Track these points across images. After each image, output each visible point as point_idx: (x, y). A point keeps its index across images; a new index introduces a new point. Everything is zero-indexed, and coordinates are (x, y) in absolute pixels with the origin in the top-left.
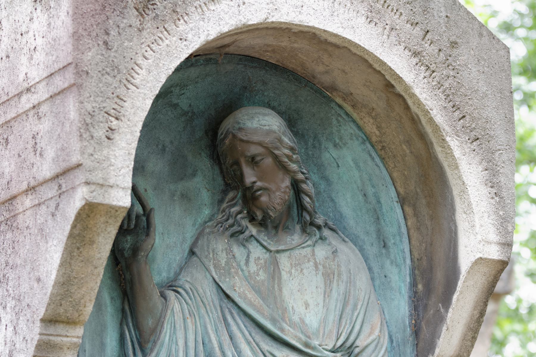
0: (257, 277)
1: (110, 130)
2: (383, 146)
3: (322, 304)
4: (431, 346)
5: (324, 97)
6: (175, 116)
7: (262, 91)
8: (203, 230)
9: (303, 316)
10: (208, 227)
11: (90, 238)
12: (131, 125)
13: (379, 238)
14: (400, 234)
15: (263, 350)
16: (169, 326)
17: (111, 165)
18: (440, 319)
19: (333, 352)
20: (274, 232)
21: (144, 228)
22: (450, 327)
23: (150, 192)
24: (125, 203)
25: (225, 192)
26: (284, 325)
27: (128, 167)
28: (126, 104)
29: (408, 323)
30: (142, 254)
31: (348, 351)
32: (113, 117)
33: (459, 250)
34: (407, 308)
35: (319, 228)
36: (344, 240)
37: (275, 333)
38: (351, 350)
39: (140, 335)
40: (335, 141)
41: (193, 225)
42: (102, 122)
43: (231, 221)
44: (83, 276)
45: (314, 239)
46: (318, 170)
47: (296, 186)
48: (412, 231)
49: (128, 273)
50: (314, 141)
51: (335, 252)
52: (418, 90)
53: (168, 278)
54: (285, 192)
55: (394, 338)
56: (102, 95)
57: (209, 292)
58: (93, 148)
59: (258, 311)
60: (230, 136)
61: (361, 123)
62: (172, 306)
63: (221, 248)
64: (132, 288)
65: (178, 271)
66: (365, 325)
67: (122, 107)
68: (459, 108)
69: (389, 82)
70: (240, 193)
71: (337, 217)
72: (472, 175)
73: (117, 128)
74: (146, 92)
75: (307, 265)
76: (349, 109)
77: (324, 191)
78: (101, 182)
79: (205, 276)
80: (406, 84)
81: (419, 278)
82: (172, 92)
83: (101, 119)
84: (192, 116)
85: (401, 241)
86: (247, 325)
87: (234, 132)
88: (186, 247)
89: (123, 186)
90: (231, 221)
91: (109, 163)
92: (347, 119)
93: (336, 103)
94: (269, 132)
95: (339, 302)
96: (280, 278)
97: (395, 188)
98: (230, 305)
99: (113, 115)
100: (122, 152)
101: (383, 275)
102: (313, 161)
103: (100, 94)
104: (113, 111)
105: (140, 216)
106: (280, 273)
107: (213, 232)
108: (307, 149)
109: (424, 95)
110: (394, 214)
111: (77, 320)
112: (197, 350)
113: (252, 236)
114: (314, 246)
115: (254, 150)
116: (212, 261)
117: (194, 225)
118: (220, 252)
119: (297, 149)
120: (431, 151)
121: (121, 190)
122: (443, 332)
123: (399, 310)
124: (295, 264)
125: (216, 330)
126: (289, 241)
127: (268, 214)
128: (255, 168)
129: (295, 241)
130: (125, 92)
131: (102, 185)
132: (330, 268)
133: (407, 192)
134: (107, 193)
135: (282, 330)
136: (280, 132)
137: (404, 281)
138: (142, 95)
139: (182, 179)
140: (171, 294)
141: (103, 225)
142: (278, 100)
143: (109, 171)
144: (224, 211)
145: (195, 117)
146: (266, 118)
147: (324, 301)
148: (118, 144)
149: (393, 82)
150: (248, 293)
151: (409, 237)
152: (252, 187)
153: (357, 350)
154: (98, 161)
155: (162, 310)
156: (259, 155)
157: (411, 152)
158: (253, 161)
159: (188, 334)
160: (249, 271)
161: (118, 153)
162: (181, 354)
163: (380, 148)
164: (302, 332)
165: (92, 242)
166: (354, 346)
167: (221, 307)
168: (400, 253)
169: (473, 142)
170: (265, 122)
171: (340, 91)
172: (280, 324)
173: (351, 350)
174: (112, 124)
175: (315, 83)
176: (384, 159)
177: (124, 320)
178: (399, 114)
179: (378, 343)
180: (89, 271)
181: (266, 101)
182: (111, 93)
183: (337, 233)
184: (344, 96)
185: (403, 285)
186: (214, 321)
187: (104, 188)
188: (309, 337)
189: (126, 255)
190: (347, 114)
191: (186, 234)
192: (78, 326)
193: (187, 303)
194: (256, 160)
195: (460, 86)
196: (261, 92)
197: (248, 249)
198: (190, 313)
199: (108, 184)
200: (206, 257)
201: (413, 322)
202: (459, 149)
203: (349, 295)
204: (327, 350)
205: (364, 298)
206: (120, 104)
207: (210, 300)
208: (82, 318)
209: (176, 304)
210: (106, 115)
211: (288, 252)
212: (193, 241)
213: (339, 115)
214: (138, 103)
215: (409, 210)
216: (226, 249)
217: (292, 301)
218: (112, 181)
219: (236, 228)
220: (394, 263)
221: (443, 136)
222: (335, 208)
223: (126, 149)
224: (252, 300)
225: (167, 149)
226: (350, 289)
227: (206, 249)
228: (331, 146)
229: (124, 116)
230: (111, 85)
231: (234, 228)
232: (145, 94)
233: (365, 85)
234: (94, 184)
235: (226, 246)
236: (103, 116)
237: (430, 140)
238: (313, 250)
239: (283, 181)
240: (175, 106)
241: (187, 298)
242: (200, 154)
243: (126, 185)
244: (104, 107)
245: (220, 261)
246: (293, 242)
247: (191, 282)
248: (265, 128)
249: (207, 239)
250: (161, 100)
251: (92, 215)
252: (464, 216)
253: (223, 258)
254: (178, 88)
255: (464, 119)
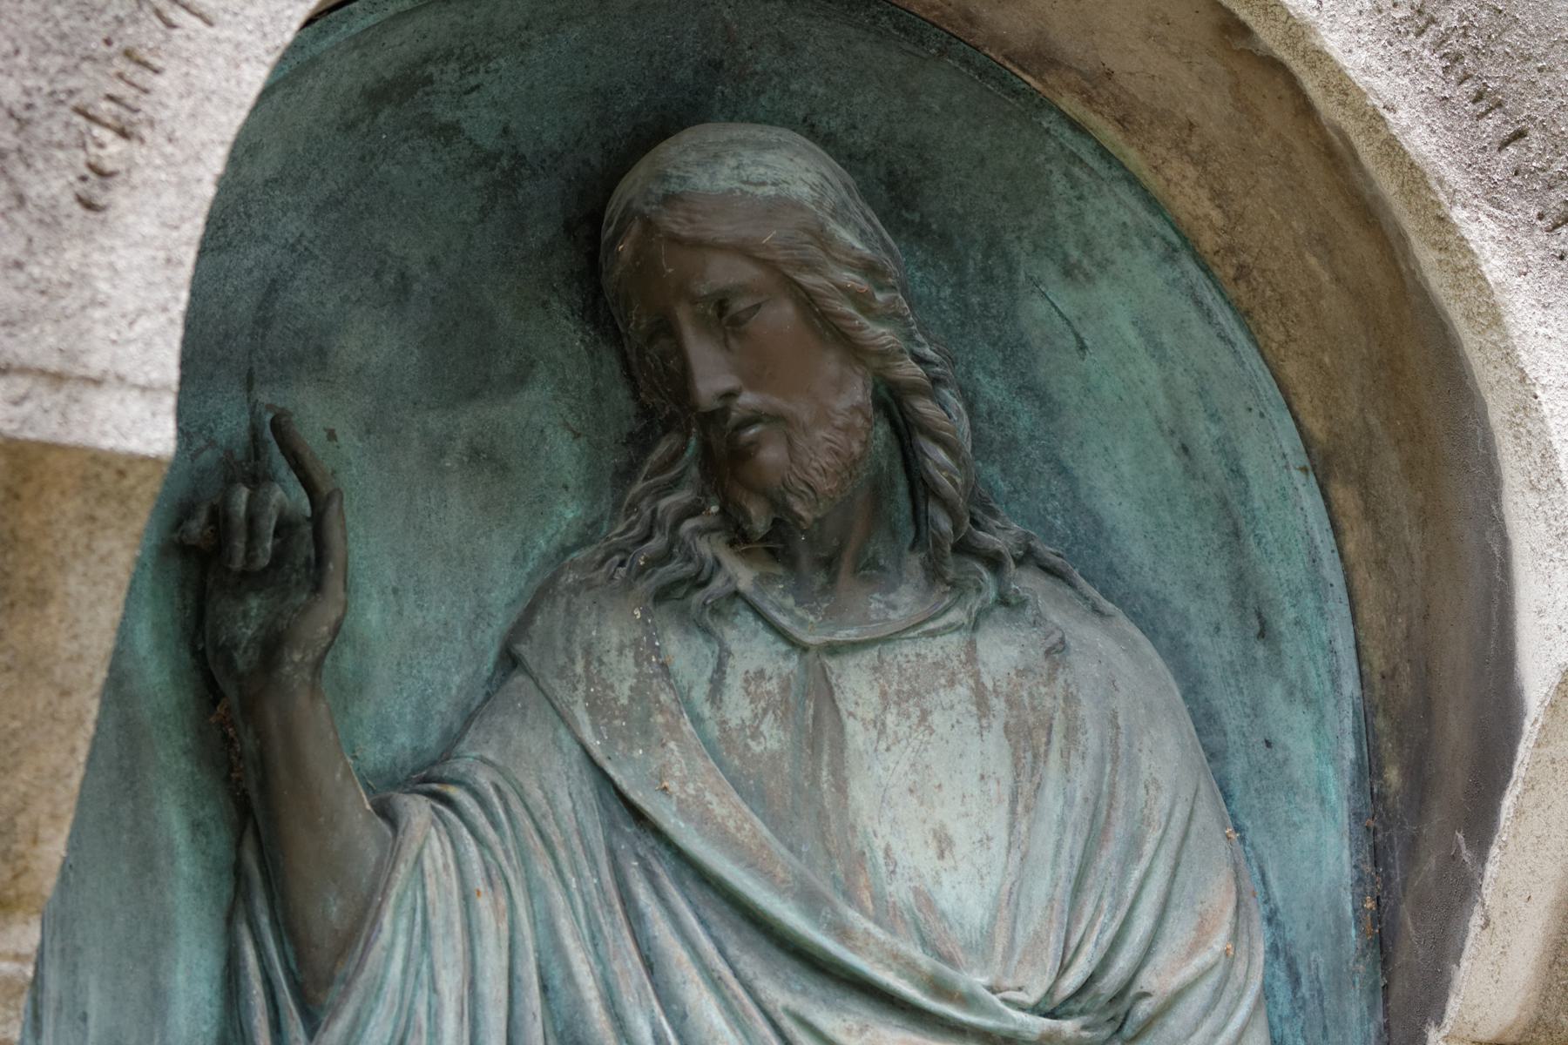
0: (752, 744)
1: (92, 176)
2: (1241, 267)
3: (1001, 836)
4: (1430, 997)
5: (1016, 93)
6: (446, 171)
7: (779, 74)
8: (554, 579)
9: (929, 881)
10: (574, 565)
11: (30, 580)
12: (179, 157)
13: (1243, 605)
14: (1318, 586)
15: (770, 1007)
16: (403, 923)
17: (95, 303)
18: (1459, 890)
19: (1051, 1015)
20: (820, 579)
21: (307, 564)
22: (1495, 915)
23: (349, 440)
24: (149, 443)
25: (640, 442)
26: (852, 915)
27: (165, 309)
28: (160, 82)
29: (1349, 908)
30: (297, 657)
31: (1111, 1014)
32: (107, 126)
33: (1518, 628)
34: (1346, 854)
35: (994, 562)
36: (1096, 610)
37: (812, 944)
38: (1121, 1009)
39: (300, 959)
40: (1066, 256)
41: (515, 559)
42: (60, 146)
43: (657, 543)
44: (16, 724)
45: (975, 603)
46: (1003, 362)
47: (892, 404)
48: (1361, 574)
49: (250, 731)
50: (987, 256)
51: (1057, 651)
52: (1335, 36)
53: (417, 752)
54: (847, 429)
55: (1302, 969)
56: (65, 46)
57: (567, 800)
58: (23, 242)
59: (752, 865)
60: (635, 228)
61: (1155, 183)
62: (415, 847)
63: (615, 640)
64: (264, 786)
65: (457, 726)
66: (1173, 915)
67: (146, 91)
68: (1500, 105)
69: (1230, 13)
70: (693, 442)
71: (1081, 530)
72: (1553, 345)
73: (121, 167)
74: (243, 37)
75: (945, 696)
76: (1109, 134)
77: (1032, 438)
78: (54, 363)
79: (556, 741)
80: (1289, 16)
81: (1387, 745)
82: (429, 80)
83: (59, 135)
84: (512, 169)
85: (1321, 612)
86: (711, 915)
87: (647, 209)
88: (488, 639)
89: (142, 381)
90: (657, 543)
91: (87, 294)
92: (1104, 173)
93: (1063, 115)
94: (779, 206)
95: (1070, 830)
96: (839, 746)
97: (1295, 418)
98: (645, 845)
99: (109, 120)
100: (140, 257)
101: (1257, 740)
102: (985, 329)
103: (55, 44)
104: (105, 105)
105: (298, 525)
106: (840, 728)
107: (589, 585)
108: (961, 285)
109: (1362, 56)
110: (1291, 516)
111: (11, 893)
112: (518, 1009)
113: (737, 594)
114: (975, 627)
115: (723, 273)
116: (581, 687)
117: (519, 559)
118: (614, 653)
119: (892, 267)
120: (1403, 267)
121: (136, 393)
122: (1472, 935)
123: (1318, 863)
124: (899, 692)
125: (593, 938)
126: (878, 611)
127: (788, 509)
128: (733, 342)
129: (901, 612)
130: (159, 36)
131: (57, 379)
132: (1034, 709)
133: (1337, 430)
134: (76, 407)
135: (843, 932)
136: (820, 205)
137: (1335, 759)
138: (228, 49)
139: (473, 395)
140: (417, 810)
141: (75, 532)
142: (843, 110)
143: (85, 324)
144: (633, 506)
145: (526, 172)
146: (768, 157)
147: (1012, 826)
148: (127, 226)
149: (1243, 14)
150: (715, 800)
151: (1350, 596)
152: (724, 412)
153: (1144, 1009)
154: (42, 286)
155: (380, 863)
156: (743, 290)
157: (1338, 280)
158: (724, 317)
159: (478, 950)
160: (723, 723)
161: (124, 257)
162: (450, 1024)
163: (1231, 272)
164: (924, 942)
165: (40, 596)
166: (1132, 993)
167: (612, 852)
168: (1319, 657)
169: (1556, 226)
170: (762, 170)
171: (1070, 68)
172: (834, 911)
173: (1121, 1009)
174: (102, 153)
175: (979, 43)
176: (1247, 313)
177: (241, 905)
178: (1280, 136)
179: (1225, 979)
180: (40, 706)
181: (800, 114)
182: (99, 39)
183: (1072, 585)
184: (1087, 85)
185: (1330, 772)
186: (586, 904)
187: (67, 389)
188: (950, 960)
189: (241, 663)
190: (1105, 154)
191: (489, 592)
192: (20, 915)
193: (480, 840)
194: (731, 312)
195: (1504, 22)
196: (776, 80)
197: (721, 644)
198: (489, 876)
199: (80, 371)
200: (561, 673)
201: (1368, 905)
202: (1503, 251)
203: (1110, 806)
204: (1021, 1007)
205: (1170, 815)
206: (137, 79)
207: (571, 826)
208: (25, 884)
209: (436, 844)
210: (78, 119)
211: (874, 652)
212: (514, 619)
213: (1075, 158)
214: (209, 77)
215: (1344, 496)
216: (636, 643)
217: (884, 829)
218: (97, 362)
219: (676, 569)
220: (1298, 695)
221: (1439, 205)
222: (1075, 498)
223: (158, 243)
224: (731, 824)
225: (417, 287)
226: (1113, 785)
227: (560, 643)
228: (1051, 273)
229: (151, 123)
230: (102, 11)
231: (670, 567)
232: (238, 45)
233: (1148, 35)
234: (24, 371)
235: (638, 632)
236: (67, 125)
237: (1396, 224)
238: (972, 644)
239: (839, 386)
240: (449, 132)
241: (481, 820)
242: (545, 304)
243: (154, 375)
244: (71, 93)
245: (612, 687)
246: (893, 615)
247: (500, 762)
248: (760, 191)
249: (568, 611)
250: (387, 111)
251: (28, 491)
252: (1532, 499)
253: (623, 677)
254: (453, 65)
255: (1523, 142)
